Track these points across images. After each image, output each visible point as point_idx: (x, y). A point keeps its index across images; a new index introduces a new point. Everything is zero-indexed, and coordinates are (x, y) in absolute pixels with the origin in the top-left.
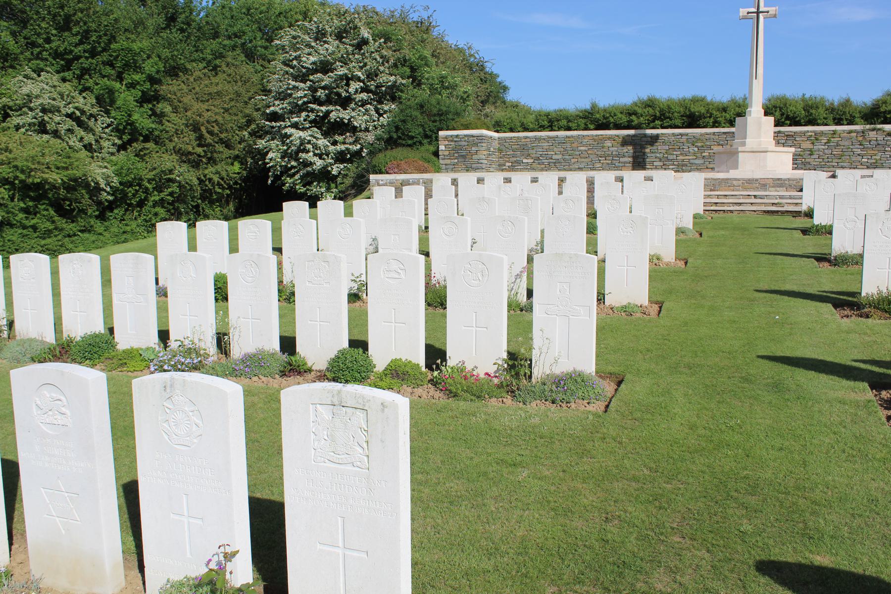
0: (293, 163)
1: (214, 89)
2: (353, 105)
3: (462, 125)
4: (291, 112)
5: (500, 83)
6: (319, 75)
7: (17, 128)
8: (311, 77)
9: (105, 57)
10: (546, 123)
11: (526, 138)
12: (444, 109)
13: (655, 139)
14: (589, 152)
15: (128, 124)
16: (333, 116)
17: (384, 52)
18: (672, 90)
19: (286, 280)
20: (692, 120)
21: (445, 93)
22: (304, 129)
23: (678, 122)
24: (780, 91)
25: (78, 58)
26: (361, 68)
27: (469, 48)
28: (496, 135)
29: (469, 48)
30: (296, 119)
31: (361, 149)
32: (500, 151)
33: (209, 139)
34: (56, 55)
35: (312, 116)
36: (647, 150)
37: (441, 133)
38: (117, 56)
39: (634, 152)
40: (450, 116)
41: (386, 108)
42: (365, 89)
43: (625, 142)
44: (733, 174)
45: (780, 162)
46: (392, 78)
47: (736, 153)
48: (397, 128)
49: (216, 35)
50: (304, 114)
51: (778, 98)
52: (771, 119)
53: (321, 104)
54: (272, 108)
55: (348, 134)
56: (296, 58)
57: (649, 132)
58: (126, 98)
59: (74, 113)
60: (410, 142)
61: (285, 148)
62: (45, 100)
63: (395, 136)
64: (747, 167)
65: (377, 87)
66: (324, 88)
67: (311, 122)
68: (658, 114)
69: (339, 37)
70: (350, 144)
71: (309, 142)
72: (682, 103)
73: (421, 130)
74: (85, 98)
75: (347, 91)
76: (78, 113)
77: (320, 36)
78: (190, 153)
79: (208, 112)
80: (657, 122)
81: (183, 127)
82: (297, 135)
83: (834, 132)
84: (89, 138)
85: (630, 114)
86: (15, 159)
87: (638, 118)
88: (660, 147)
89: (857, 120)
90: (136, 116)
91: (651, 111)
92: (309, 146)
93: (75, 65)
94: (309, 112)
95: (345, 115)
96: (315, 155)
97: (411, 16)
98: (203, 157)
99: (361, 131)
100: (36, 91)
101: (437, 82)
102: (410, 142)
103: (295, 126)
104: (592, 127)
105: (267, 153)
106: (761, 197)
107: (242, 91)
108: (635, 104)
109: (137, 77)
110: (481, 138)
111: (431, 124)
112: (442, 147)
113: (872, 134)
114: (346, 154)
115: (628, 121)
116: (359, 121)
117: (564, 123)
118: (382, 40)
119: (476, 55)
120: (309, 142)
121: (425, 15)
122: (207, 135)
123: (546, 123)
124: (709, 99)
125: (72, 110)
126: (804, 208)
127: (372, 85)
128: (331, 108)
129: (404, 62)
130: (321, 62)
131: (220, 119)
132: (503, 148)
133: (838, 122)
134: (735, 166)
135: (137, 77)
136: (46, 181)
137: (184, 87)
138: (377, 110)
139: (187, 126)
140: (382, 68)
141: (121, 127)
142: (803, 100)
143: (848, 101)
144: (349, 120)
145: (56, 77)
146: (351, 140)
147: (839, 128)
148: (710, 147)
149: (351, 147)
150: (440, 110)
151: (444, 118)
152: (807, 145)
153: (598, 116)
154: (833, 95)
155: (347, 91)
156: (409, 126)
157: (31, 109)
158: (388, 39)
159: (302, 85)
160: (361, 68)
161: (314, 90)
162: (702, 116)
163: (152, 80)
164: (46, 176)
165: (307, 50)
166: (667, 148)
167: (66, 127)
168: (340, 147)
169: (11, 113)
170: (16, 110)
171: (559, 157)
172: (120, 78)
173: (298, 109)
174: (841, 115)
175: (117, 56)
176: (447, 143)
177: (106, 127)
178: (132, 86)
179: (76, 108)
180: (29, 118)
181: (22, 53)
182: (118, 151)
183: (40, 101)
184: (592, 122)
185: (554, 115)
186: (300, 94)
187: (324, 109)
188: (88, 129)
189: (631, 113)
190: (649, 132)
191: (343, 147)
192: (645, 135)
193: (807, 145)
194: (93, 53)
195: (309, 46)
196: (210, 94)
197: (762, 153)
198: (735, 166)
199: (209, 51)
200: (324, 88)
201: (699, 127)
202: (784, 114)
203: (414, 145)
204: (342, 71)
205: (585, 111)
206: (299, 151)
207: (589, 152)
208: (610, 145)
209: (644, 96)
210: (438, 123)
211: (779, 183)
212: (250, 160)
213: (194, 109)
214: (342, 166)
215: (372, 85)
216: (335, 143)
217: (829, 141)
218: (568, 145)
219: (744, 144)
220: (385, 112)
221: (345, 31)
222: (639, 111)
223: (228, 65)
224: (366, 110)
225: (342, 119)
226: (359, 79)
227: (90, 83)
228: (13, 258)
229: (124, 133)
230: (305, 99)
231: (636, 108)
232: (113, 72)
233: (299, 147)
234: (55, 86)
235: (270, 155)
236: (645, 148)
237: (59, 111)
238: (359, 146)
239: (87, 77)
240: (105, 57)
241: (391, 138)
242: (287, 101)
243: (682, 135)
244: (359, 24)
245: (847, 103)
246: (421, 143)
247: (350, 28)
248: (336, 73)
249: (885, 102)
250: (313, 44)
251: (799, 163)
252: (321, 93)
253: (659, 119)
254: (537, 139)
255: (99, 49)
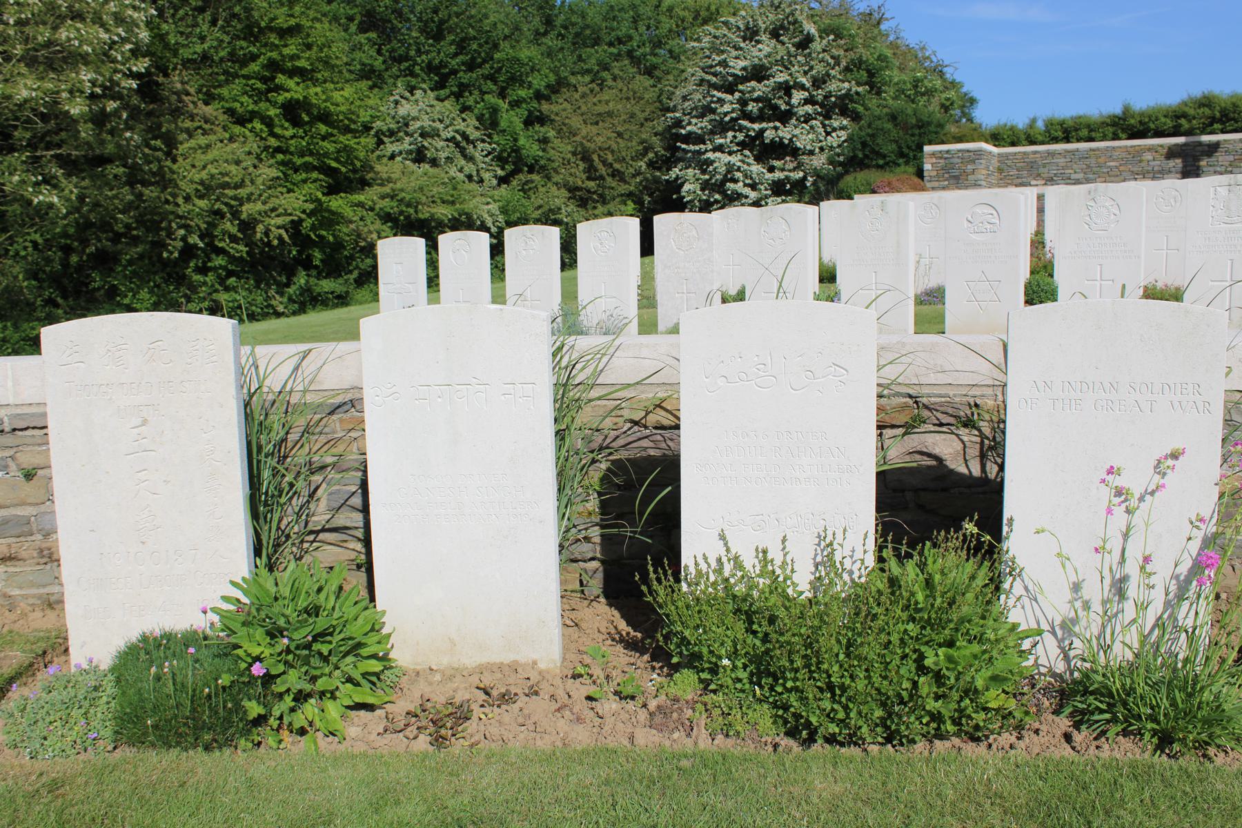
0: (717, 196)
1: (601, 108)
2: (793, 121)
3: (954, 138)
4: (712, 132)
5: (966, 94)
6: (753, 83)
7: (392, 157)
8: (740, 87)
9: (486, 69)
11: (1035, 153)
13: (1213, 148)
14: (1122, 168)
15: (513, 151)
16: (769, 135)
17: (835, 52)
22: (730, 153)
25: (454, 72)
26: (806, 73)
27: (923, 49)
28: (995, 150)
29: (923, 49)
30: (722, 141)
31: (805, 178)
32: (1000, 170)
33: (603, 170)
34: (430, 68)
35: (740, 136)
36: (1203, 163)
37: (927, 148)
38: (500, 68)
39: (1184, 167)
40: (932, 128)
41: (836, 124)
42: (810, 101)
43: (1172, 153)
46: (846, 85)
48: (864, 144)
49: (597, 42)
50: (730, 134)
53: (752, 121)
54: (689, 128)
55: (788, 158)
56: (720, 64)
57: (1206, 138)
58: (511, 119)
59: (454, 138)
60: (881, 162)
61: (707, 177)
62: (426, 123)
65: (826, 97)
66: (757, 100)
67: (738, 144)
68: (1218, 115)
69: (775, 34)
70: (790, 171)
71: (739, 169)
73: (894, 146)
74: (464, 120)
75: (788, 103)
76: (459, 138)
77: (751, 34)
78: (578, 189)
79: (600, 137)
80: (1216, 126)
81: (569, 156)
82: (721, 161)
84: (470, 168)
86: (402, 190)
87: (1190, 121)
88: (1221, 158)
90: (522, 141)
91: (1207, 111)
92: (738, 175)
93: (452, 81)
94: (735, 131)
95: (785, 133)
96: (745, 185)
97: (856, 7)
98: (594, 193)
99: (804, 154)
100: (414, 113)
101: (909, 86)
102: (881, 162)
103: (719, 149)
104: (1124, 136)
105: (682, 185)
107: (636, 109)
109: (522, 93)
110: (979, 153)
112: (927, 167)
115: (1174, 127)
116: (804, 140)
117: (1084, 133)
118: (832, 37)
119: (934, 59)
120: (739, 169)
122: (600, 166)
125: (452, 134)
127: (819, 95)
128: (764, 125)
129: (858, 64)
130: (754, 67)
131: (615, 147)
132: (1003, 166)
135: (522, 93)
136: (432, 215)
137: (569, 106)
138: (824, 126)
139: (574, 154)
140: (833, 72)
141: (505, 155)
144: (791, 140)
145: (432, 95)
146: (791, 166)
149: (792, 174)
151: (927, 131)
153: (1132, 121)
156: (879, 141)
157: (407, 134)
158: (838, 36)
159: (728, 97)
160: (806, 73)
161: (743, 102)
163: (539, 96)
164: (434, 211)
165: (734, 53)
166: (1231, 158)
167: (446, 154)
168: (778, 175)
169: (385, 139)
170: (390, 137)
172: (502, 94)
173: (722, 127)
175: (500, 68)
176: (934, 160)
177: (486, 156)
178: (515, 104)
179: (457, 131)
180: (406, 145)
181: (386, 70)
182: (499, 185)
183: (418, 124)
184: (1123, 130)
185: (1071, 123)
186: (727, 108)
187: (756, 126)
188: (470, 159)
190: (1206, 138)
192: (1200, 144)
194: (471, 66)
195: (737, 48)
196: (600, 114)
199: (594, 61)
200: (757, 100)
204: (782, 77)
205: (1115, 116)
206: (725, 180)
207: (1122, 168)
208: (1150, 158)
209: (1197, 91)
212: (647, 199)
213: (584, 132)
215: (819, 95)
216: (771, 169)
220: (834, 130)
221: (782, 27)
222: (1192, 112)
223: (615, 79)
224: (812, 127)
225: (781, 139)
226: (802, 87)
227: (470, 102)
228: (661, 222)
229: (507, 162)
230: (734, 115)
231: (1187, 109)
232: (494, 88)
233: (726, 175)
234: (432, 106)
235: (687, 187)
236: (1199, 160)
237: (439, 136)
238: (801, 174)
239: (467, 94)
240: (486, 69)
241: (855, 156)
242: (707, 118)
244: (800, 18)
247: (789, 23)
248: (772, 80)
250: (742, 45)
252: (752, 107)
253: (1220, 121)
254: (1051, 154)
255: (479, 60)
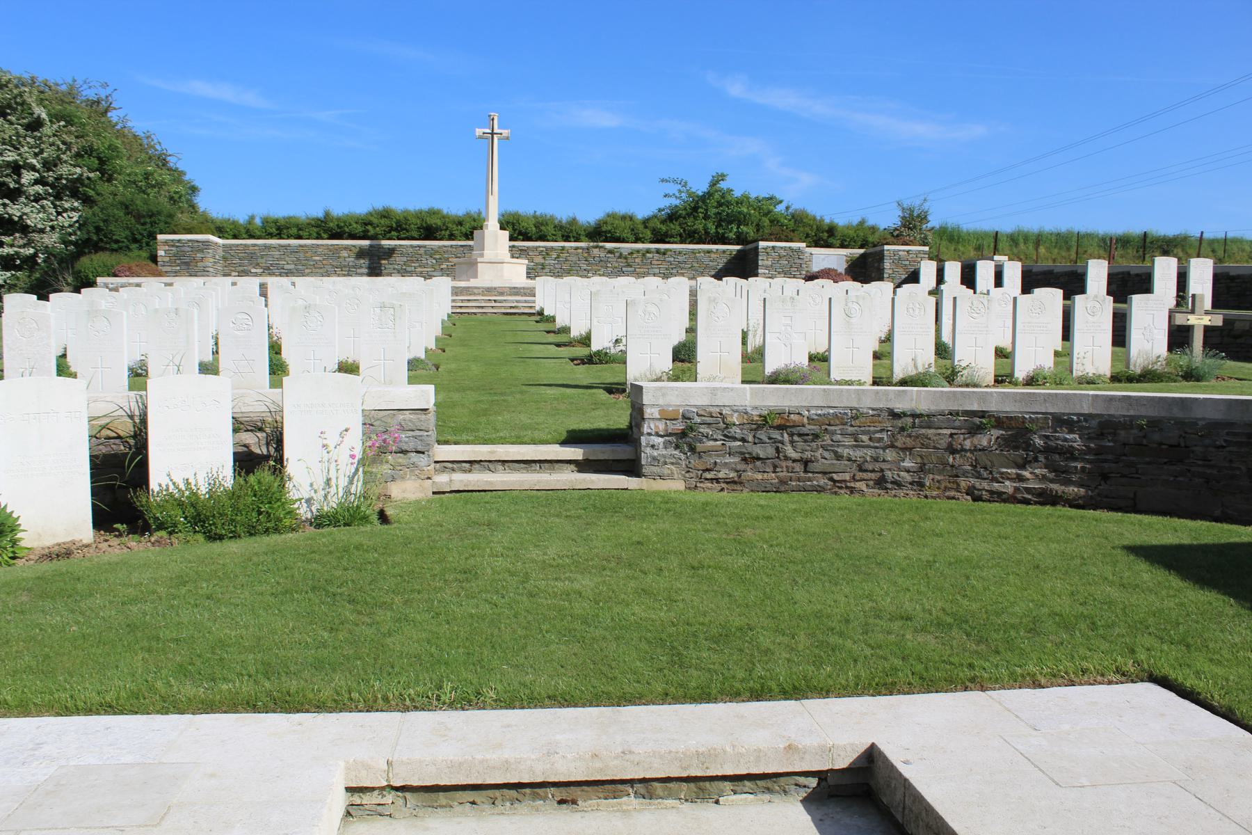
2: (23, 199)
10: (274, 230)
11: (255, 245)
12: (155, 210)
13: (391, 252)
18: (408, 200)
19: (274, 331)
20: (429, 232)
21: (152, 192)
23: (415, 234)
24: (513, 207)
28: (220, 241)
29: (148, 137)
31: (35, 255)
32: (225, 259)
37: (160, 237)
41: (67, 205)
43: (361, 254)
44: (473, 283)
45: (515, 273)
46: (78, 170)
47: (475, 264)
51: (510, 214)
52: (506, 234)
60: (115, 246)
63: (95, 238)
64: (486, 277)
70: (20, 247)
72: (419, 214)
75: (18, 182)
83: (563, 248)
85: (366, 224)
88: (398, 259)
89: (583, 238)
91: (387, 222)
102: (115, 246)
104: (325, 236)
106: (500, 302)
108: (371, 214)
110: (207, 244)
111: (140, 227)
112: (161, 253)
113: (596, 251)
114: (14, 260)
116: (34, 218)
118: (62, 123)
121: (103, 94)
123: (274, 230)
124: (445, 212)
126: (538, 308)
129: (89, 151)
133: (566, 238)
134: (476, 276)
140: (64, 157)
142: (535, 217)
143: (574, 219)
144: (20, 217)
146: (21, 242)
147: (567, 244)
148: (447, 260)
150: (150, 210)
152: (539, 259)
154: (561, 212)
155: (18, 182)
158: (69, 122)
162: (438, 229)
171: (292, 267)
174: (568, 232)
184: (325, 231)
185: (283, 222)
189: (367, 223)
190: (385, 243)
191: (11, 251)
192: (380, 247)
193: (539, 259)
197: (499, 264)
198: (476, 276)
201: (435, 239)
202: (517, 229)
203: (119, 248)
210: (148, 226)
211: (515, 291)
214: (8, 274)
217: (558, 257)
218: (302, 255)
219: (482, 255)
220: (66, 210)
222: (375, 221)
224: (42, 207)
226: (33, 168)
238: (32, 251)
243: (420, 247)
244: (29, 100)
245: (573, 221)
246: (128, 247)
247: (16, 103)
249: (606, 223)
251: (531, 274)
253: (396, 230)
